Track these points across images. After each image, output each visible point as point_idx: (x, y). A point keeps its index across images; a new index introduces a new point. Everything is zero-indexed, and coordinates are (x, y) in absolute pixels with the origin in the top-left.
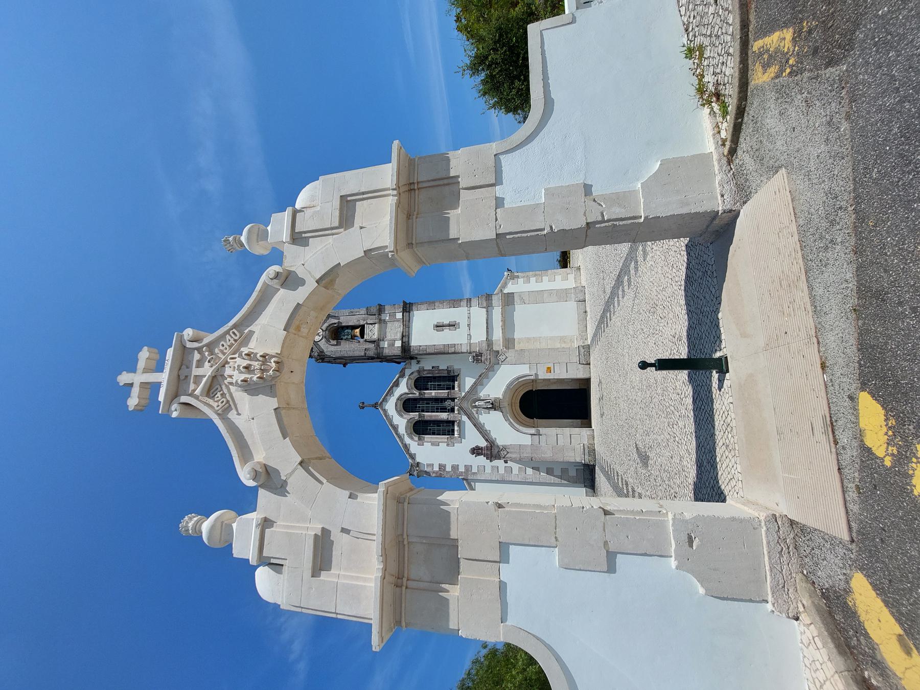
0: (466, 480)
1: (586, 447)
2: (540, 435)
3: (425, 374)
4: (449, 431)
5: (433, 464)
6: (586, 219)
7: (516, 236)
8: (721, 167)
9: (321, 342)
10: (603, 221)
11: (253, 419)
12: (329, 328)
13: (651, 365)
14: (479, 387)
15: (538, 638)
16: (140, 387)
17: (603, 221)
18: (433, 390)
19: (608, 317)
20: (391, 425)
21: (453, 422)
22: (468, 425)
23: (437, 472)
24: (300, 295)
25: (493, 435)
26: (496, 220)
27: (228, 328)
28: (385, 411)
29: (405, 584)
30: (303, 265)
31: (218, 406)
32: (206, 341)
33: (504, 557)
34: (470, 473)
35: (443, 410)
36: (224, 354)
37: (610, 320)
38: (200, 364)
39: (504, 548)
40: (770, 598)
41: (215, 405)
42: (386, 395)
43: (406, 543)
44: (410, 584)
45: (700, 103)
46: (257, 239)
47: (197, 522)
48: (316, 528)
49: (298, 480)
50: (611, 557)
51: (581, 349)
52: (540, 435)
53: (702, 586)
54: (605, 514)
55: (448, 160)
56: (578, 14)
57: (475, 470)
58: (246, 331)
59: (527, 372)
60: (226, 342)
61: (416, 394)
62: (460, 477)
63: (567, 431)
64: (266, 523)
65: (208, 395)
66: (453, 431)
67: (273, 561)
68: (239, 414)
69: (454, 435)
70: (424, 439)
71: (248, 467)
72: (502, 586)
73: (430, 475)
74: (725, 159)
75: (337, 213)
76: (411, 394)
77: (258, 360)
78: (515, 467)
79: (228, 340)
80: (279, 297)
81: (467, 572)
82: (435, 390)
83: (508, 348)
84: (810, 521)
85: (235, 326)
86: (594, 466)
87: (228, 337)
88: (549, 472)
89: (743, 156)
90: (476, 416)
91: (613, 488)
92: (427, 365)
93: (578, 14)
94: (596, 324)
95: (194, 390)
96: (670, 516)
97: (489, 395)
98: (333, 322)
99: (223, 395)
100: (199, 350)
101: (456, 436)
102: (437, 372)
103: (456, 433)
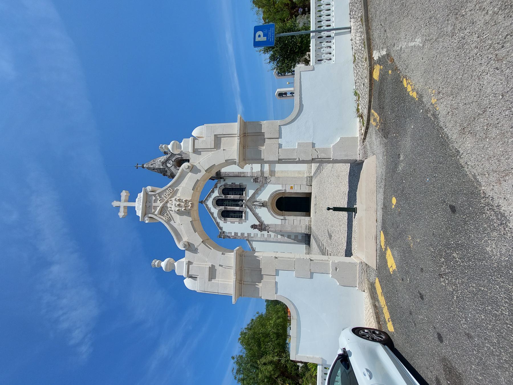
0: (248, 240)
1: (307, 226)
2: (285, 220)
3: (228, 187)
4: (240, 216)
5: (231, 232)
6: (312, 157)
7: (286, 160)
8: (360, 143)
9: (172, 168)
10: (318, 158)
11: (182, 225)
12: (176, 160)
13: (331, 209)
14: (256, 195)
15: (287, 298)
16: (124, 208)
17: (318, 158)
18: (232, 195)
19: (322, 168)
20: (210, 213)
21: (242, 212)
22: (250, 213)
23: (233, 236)
24: (199, 176)
25: (263, 219)
26: (279, 153)
27: (167, 187)
28: (207, 205)
29: (243, 283)
30: (199, 163)
31: (165, 219)
32: (157, 192)
33: (277, 274)
34: (250, 237)
35: (237, 205)
36: (166, 198)
37: (324, 168)
38: (155, 201)
39: (277, 271)
40: (357, 286)
41: (164, 218)
42: (207, 197)
43: (243, 269)
44: (244, 283)
45: (357, 115)
46: (176, 148)
47: (159, 263)
48: (210, 265)
49: (202, 248)
50: (312, 274)
51: (308, 178)
52: (285, 220)
53: (338, 282)
54: (311, 261)
55: (261, 125)
56: (316, 66)
57: (252, 235)
58: (175, 189)
59: (281, 188)
60: (166, 193)
61: (223, 197)
62: (245, 239)
63: (299, 218)
64: (189, 263)
65: (160, 214)
66: (242, 216)
67: (193, 276)
68: (175, 222)
69: (242, 218)
70: (227, 220)
71: (181, 243)
72: (276, 283)
73: (230, 238)
74: (362, 140)
75: (213, 142)
76: (221, 197)
77: (183, 202)
78: (272, 234)
79: (167, 193)
80: (189, 176)
81: (265, 279)
82: (233, 195)
83: (271, 176)
84: (370, 265)
85: (170, 187)
86: (310, 235)
87: (167, 191)
88: (289, 237)
89: (367, 142)
90: (254, 209)
91: (318, 246)
92: (229, 182)
93: (316, 66)
94: (316, 168)
95: (155, 212)
96: (331, 261)
97: (261, 199)
98: (178, 157)
99: (167, 215)
100: (155, 195)
101: (243, 218)
102: (234, 186)
103: (243, 217)
